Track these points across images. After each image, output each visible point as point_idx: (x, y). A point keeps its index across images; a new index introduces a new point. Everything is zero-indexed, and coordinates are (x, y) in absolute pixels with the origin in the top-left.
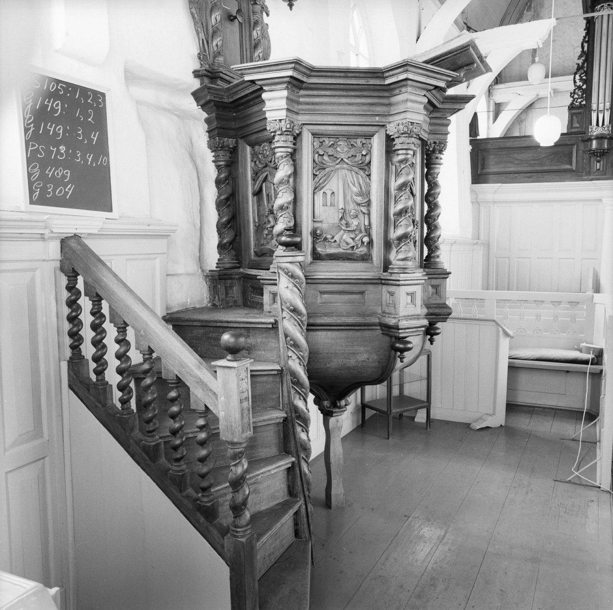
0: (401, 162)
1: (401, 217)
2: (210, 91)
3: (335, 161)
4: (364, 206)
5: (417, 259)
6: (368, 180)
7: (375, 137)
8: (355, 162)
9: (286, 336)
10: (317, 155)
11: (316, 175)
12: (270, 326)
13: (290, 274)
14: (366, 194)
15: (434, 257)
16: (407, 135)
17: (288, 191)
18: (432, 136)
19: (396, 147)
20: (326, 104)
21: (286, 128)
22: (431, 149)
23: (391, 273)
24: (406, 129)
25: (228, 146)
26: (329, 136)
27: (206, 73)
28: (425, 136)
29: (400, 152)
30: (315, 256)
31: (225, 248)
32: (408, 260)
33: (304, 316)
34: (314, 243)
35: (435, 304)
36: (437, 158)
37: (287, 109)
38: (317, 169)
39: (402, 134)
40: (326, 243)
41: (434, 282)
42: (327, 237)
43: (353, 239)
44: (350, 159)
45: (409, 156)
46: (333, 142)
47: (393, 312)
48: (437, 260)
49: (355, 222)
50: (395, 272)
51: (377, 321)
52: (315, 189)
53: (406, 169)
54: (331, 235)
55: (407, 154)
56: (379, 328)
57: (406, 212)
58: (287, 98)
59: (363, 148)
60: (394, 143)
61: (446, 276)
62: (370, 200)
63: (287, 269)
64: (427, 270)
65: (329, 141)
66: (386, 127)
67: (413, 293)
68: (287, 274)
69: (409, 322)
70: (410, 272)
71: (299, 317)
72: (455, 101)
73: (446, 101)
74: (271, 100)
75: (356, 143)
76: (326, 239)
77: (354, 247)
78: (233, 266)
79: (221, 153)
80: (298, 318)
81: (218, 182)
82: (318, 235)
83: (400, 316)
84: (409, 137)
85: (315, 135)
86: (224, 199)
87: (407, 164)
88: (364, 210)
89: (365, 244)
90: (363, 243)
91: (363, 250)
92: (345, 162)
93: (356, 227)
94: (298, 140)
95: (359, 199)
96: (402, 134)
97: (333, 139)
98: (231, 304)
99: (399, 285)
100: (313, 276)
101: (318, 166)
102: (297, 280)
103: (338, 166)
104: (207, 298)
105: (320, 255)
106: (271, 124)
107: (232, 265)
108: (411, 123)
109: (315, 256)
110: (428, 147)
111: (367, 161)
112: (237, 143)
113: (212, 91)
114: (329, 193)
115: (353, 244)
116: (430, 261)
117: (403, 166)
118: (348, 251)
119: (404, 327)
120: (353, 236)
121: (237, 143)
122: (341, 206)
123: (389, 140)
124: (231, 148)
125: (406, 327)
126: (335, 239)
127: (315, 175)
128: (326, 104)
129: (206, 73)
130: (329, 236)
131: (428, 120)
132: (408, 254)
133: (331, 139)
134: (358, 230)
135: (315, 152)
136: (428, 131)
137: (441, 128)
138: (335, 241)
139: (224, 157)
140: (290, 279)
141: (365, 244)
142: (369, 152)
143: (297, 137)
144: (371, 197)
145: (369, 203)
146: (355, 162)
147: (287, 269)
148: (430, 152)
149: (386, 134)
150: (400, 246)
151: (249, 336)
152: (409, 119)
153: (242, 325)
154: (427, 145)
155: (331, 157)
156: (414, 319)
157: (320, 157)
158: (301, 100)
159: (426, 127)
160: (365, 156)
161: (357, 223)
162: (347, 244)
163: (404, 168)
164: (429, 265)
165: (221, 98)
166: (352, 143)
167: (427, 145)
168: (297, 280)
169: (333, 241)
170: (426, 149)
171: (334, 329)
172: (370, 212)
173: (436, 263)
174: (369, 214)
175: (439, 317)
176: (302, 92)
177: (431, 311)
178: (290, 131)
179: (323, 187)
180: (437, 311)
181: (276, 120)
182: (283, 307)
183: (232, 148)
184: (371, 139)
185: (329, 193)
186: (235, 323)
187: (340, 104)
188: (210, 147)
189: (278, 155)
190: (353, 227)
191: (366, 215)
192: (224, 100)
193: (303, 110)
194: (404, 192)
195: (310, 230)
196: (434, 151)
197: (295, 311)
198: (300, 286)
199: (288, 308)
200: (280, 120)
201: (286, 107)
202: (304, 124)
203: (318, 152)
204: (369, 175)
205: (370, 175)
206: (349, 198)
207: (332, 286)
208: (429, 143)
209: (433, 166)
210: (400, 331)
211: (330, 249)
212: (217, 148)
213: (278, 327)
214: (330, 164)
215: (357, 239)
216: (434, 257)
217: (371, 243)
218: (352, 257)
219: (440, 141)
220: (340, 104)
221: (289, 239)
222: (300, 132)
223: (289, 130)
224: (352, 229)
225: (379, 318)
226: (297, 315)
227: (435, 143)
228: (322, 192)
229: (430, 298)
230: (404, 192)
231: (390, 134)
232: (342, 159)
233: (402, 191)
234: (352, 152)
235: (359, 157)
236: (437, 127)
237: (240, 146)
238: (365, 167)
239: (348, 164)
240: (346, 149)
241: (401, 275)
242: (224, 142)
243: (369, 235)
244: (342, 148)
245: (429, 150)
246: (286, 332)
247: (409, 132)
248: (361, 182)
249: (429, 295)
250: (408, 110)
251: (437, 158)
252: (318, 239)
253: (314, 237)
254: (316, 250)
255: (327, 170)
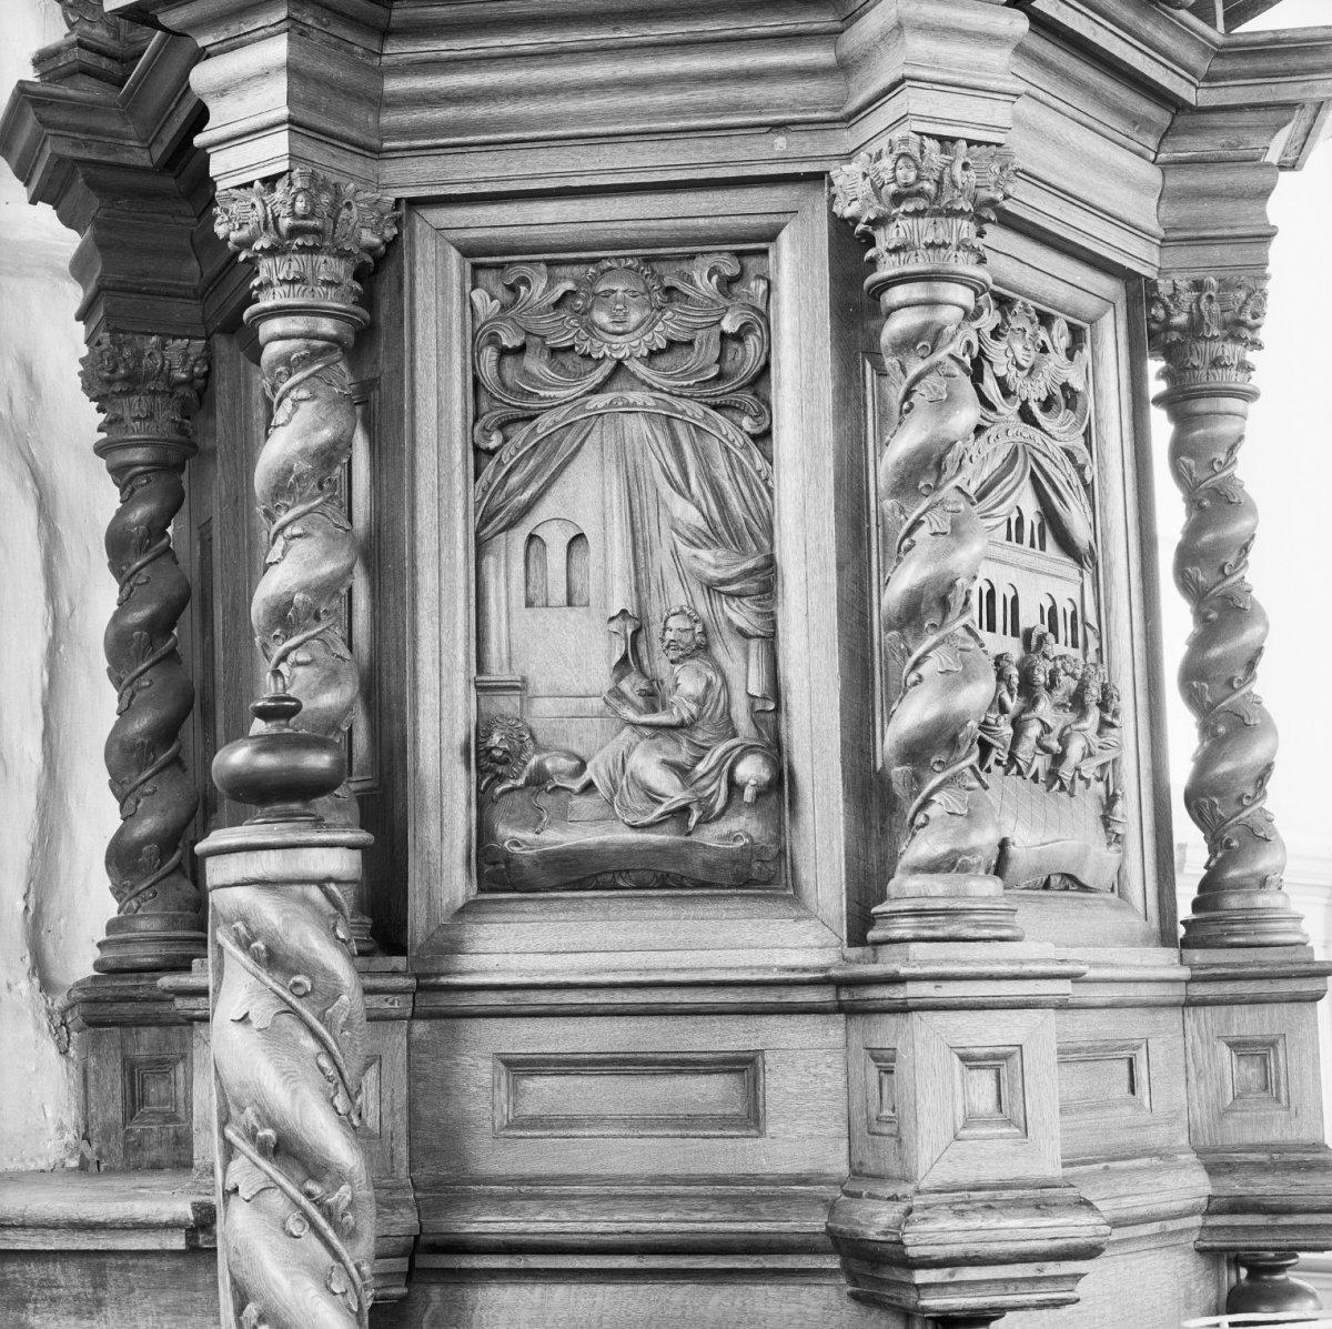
0: (906, 344)
1: (919, 636)
2: (47, 114)
3: (580, 376)
4: (739, 595)
5: (1135, 891)
6: (760, 462)
7: (784, 236)
8: (687, 374)
9: (242, 1297)
10: (489, 355)
11: (491, 453)
12: (178, 1242)
13: (260, 945)
14: (746, 536)
15: (1239, 886)
16: (922, 204)
17: (318, 534)
18: (1184, 256)
19: (885, 271)
20: (516, 93)
21: (293, 214)
22: (1181, 319)
23: (877, 943)
24: (907, 174)
25: (165, 373)
26: (553, 255)
27: (88, 58)
28: (1139, 255)
29: (897, 295)
30: (488, 869)
31: (135, 869)
32: (965, 868)
33: (341, 1178)
34: (484, 802)
35: (1254, 1148)
36: (1216, 363)
37: (290, 121)
38: (490, 418)
39: (897, 199)
40: (545, 801)
41: (1247, 1022)
42: (549, 765)
43: (682, 771)
44: (662, 362)
45: (949, 315)
46: (569, 286)
47: (893, 1167)
48: (1261, 900)
49: (688, 682)
50: (897, 934)
51: (816, 1223)
52: (485, 520)
53: (931, 380)
54: (571, 755)
55: (933, 303)
56: (833, 1263)
57: (944, 604)
58: (292, 70)
59: (724, 302)
60: (870, 253)
61: (1306, 986)
62: (770, 564)
63: (245, 920)
64: (1198, 956)
65: (552, 281)
66: (831, 184)
67: (1005, 1057)
68: (245, 944)
69: (976, 1221)
70: (970, 933)
71: (311, 1186)
72: (1279, 64)
73: (1228, 66)
74: (225, 90)
75: (690, 280)
76: (539, 779)
77: (684, 811)
78: (168, 957)
79: (136, 405)
80: (309, 1195)
81: (120, 545)
82: (498, 754)
83: (924, 1185)
84: (938, 213)
85: (482, 258)
86: (138, 626)
87: (940, 356)
88: (742, 615)
89: (749, 794)
90: (734, 787)
91: (742, 827)
92: (633, 375)
93: (694, 708)
94: (385, 288)
95: (712, 562)
96: (897, 199)
97: (576, 270)
98: (152, 1155)
99: (904, 1009)
100: (484, 972)
101: (498, 412)
102: (298, 979)
103: (599, 401)
104: (61, 1128)
105: (508, 859)
106: (234, 207)
107: (173, 951)
108: (941, 139)
109: (488, 869)
110: (1161, 314)
111: (751, 364)
112: (209, 357)
113: (62, 117)
114: (557, 539)
115: (673, 792)
116: (1217, 908)
117: (916, 367)
118: (654, 838)
119: (940, 1252)
120: (683, 756)
121: (209, 357)
122: (620, 599)
123: (850, 244)
124: (182, 383)
125: (955, 1250)
126: (588, 774)
127: (481, 454)
128: (516, 93)
129: (88, 58)
130: (556, 763)
131: (1152, 174)
132: (966, 833)
133: (564, 270)
134: (712, 718)
135: (480, 337)
136: (1162, 234)
137: (1225, 209)
138: (589, 787)
139: (151, 424)
140: (264, 975)
141: (749, 794)
142: (761, 320)
143: (378, 275)
144: (777, 551)
145: (765, 582)
146: (687, 374)
147: (245, 920)
148: (1175, 336)
149: (832, 215)
150: (924, 793)
151: (100, 1303)
152: (922, 118)
153: (56, 1242)
154: (1153, 300)
155: (568, 360)
156: (1017, 1204)
157: (508, 360)
158: (393, 85)
159: (1145, 211)
160: (739, 337)
161: (701, 686)
162: (653, 796)
163: (918, 378)
164: (1214, 930)
165: (112, 149)
166: (667, 282)
167: (1153, 300)
168: (298, 979)
169: (577, 785)
170: (1154, 319)
171: (591, 1271)
172: (774, 624)
173: (1251, 917)
174: (770, 640)
175: (1286, 1220)
176: (398, 50)
177: (1235, 1186)
178: (315, 231)
179: (528, 508)
180: (1266, 1186)
181: (251, 184)
182: (230, 1133)
183: (189, 382)
184: (765, 252)
185: (557, 539)
186: (23, 1226)
187: (582, 89)
188: (87, 388)
189: (272, 350)
190: (681, 710)
191: (754, 643)
192: (126, 158)
193: (403, 133)
194: (926, 503)
195: (460, 729)
196: (1195, 328)
197: (285, 1149)
198: (321, 1018)
199: (252, 1136)
200: (270, 182)
201: (284, 112)
202: (414, 203)
203: (493, 339)
204: (763, 437)
205: (767, 434)
206: (662, 559)
207: (604, 1025)
208: (1164, 288)
209: (1203, 406)
210: (921, 1277)
211: (563, 831)
212: (109, 382)
213: (215, 1249)
214: (561, 393)
215: (701, 768)
216: (1239, 886)
217: (781, 789)
218: (681, 869)
219: (1227, 275)
220: (582, 89)
221: (266, 761)
222: (393, 244)
223: (310, 223)
224: (675, 720)
225: (832, 1207)
226: (299, 1176)
227: (1198, 286)
228: (519, 536)
229: (1224, 1113)
230: (926, 503)
231: (848, 212)
232: (620, 363)
233: (918, 494)
234: (669, 325)
235: (706, 353)
236: (1204, 208)
237: (221, 369)
238: (746, 391)
239: (651, 388)
240: (635, 317)
241: (917, 949)
242: (138, 355)
243: (775, 749)
244: (624, 324)
245: (1167, 327)
246: (239, 1274)
247: (928, 186)
248: (722, 471)
249: (1220, 1093)
250: (919, 73)
251: (1216, 363)
252: (501, 778)
253: (481, 771)
254: (493, 837)
255: (545, 422)
